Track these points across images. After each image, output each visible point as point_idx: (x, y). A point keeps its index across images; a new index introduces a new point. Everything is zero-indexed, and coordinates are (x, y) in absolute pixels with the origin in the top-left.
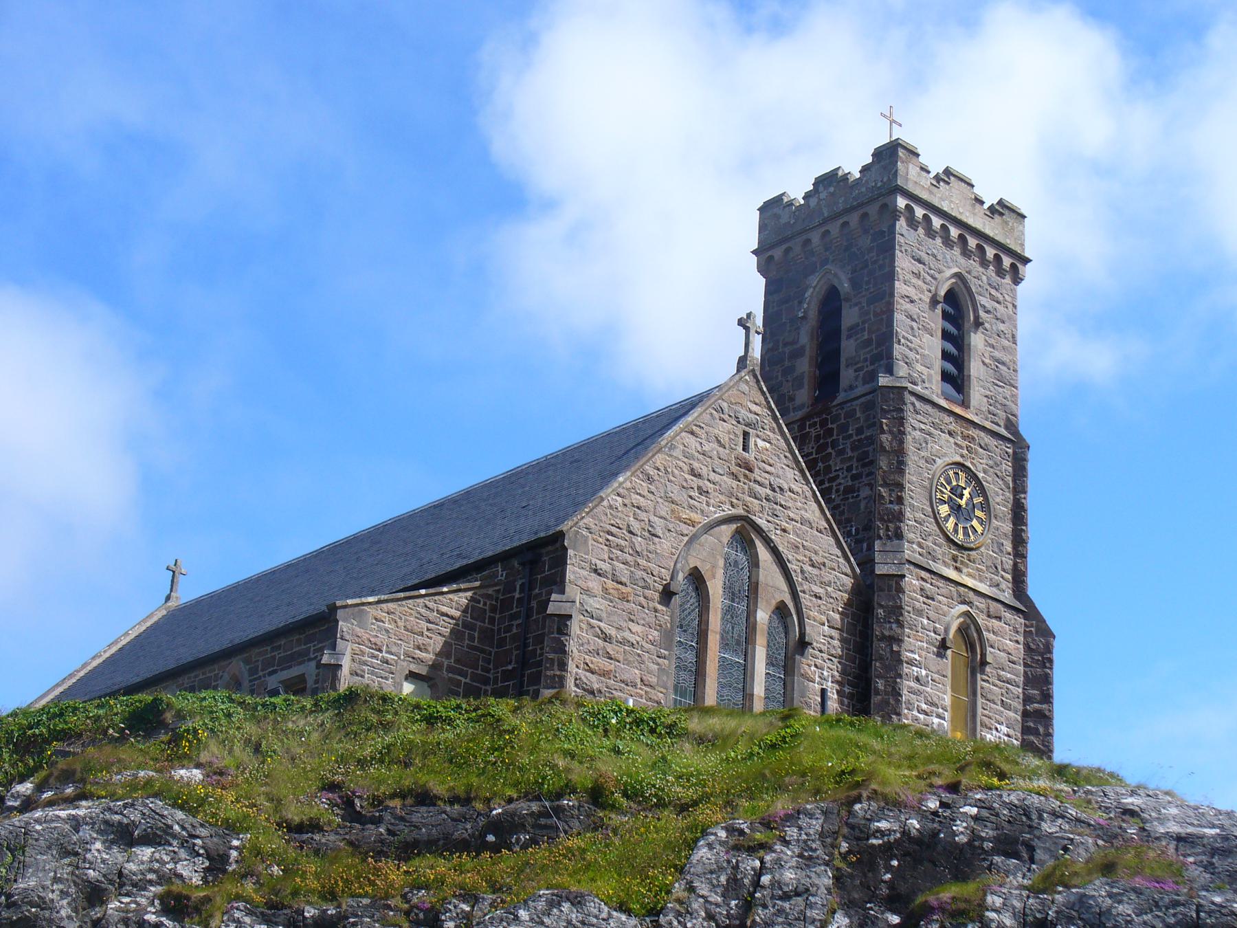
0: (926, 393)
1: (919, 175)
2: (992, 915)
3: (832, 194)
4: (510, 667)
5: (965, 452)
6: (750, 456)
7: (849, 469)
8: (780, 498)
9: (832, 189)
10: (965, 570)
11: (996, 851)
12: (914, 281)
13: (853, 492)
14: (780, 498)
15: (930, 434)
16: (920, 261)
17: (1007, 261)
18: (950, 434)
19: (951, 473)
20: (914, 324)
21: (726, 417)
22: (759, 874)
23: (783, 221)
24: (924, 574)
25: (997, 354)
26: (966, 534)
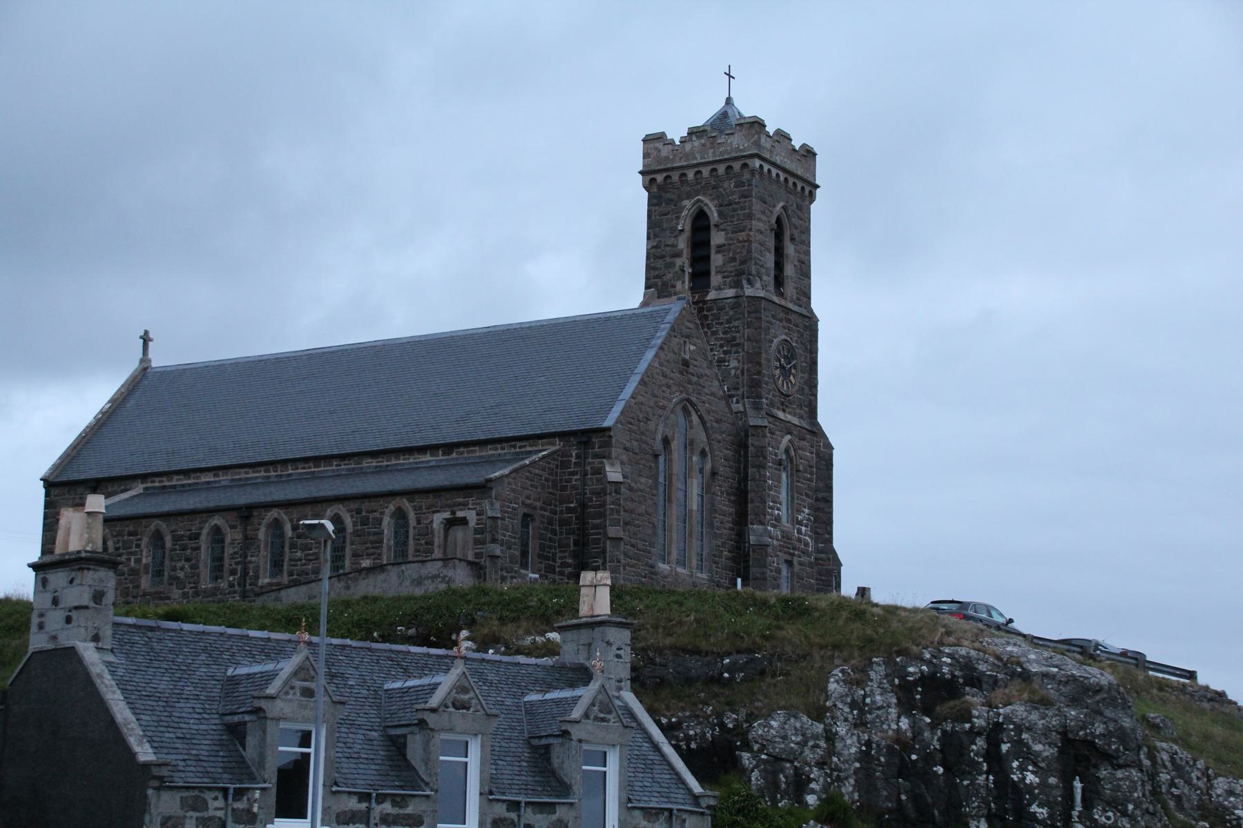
2: (975, 720)
3: (703, 145)
4: (572, 505)
9: (703, 141)
10: (787, 410)
11: (965, 684)
13: (725, 361)
20: (762, 248)
22: (865, 697)
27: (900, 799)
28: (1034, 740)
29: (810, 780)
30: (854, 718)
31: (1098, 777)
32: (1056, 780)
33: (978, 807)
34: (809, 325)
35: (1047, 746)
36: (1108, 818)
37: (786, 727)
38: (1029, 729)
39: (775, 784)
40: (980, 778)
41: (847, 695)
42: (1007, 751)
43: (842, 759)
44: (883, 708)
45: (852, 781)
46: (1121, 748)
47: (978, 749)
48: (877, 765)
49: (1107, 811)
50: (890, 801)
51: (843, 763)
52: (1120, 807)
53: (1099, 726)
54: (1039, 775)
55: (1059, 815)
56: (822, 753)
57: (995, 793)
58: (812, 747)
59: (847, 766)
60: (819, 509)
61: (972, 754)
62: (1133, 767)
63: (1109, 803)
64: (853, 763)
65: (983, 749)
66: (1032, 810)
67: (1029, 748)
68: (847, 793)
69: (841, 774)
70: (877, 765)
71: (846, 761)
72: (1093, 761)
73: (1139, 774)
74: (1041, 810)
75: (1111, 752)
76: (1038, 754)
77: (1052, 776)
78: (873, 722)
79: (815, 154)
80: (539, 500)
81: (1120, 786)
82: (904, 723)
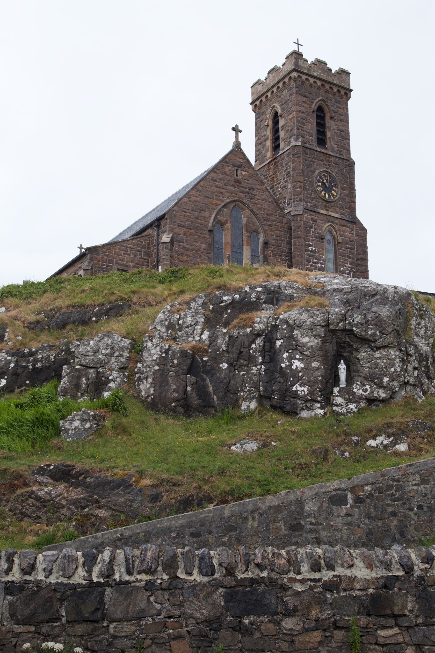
0: (310, 147)
1: (303, 63)
3: (274, 77)
5: (327, 166)
6: (239, 177)
7: (284, 179)
8: (253, 192)
12: (304, 104)
14: (253, 192)
15: (312, 161)
16: (305, 96)
17: (342, 92)
18: (321, 161)
19: (322, 175)
20: (304, 121)
21: (229, 165)
22: (179, 319)
23: (259, 90)
24: (312, 213)
25: (340, 128)
26: (329, 196)
27: (186, 390)
28: (302, 335)
29: (109, 381)
30: (167, 336)
31: (358, 359)
32: (318, 364)
33: (249, 391)
34: (351, 165)
35: (312, 338)
36: (365, 391)
37: (100, 344)
38: (299, 327)
39: (77, 386)
40: (254, 368)
41: (166, 320)
42: (281, 346)
43: (145, 364)
44: (192, 326)
45: (150, 380)
46: (378, 332)
47: (257, 347)
48: (171, 366)
49: (365, 385)
50: (177, 392)
51: (145, 367)
52: (376, 381)
53: (357, 317)
54: (304, 361)
55: (320, 391)
56: (124, 360)
57: (265, 378)
58: (117, 357)
59: (148, 369)
60: (359, 264)
61: (251, 351)
62: (391, 347)
63: (366, 378)
64: (153, 366)
65: (260, 346)
66: (294, 389)
67: (297, 340)
68: (144, 390)
69: (141, 376)
70: (171, 366)
71: (149, 366)
72: (355, 346)
73: (397, 353)
74: (303, 388)
75: (367, 337)
76: (304, 345)
77: (315, 361)
78: (182, 336)
79: (349, 74)
80: (132, 262)
81: (377, 364)
82: (206, 336)
